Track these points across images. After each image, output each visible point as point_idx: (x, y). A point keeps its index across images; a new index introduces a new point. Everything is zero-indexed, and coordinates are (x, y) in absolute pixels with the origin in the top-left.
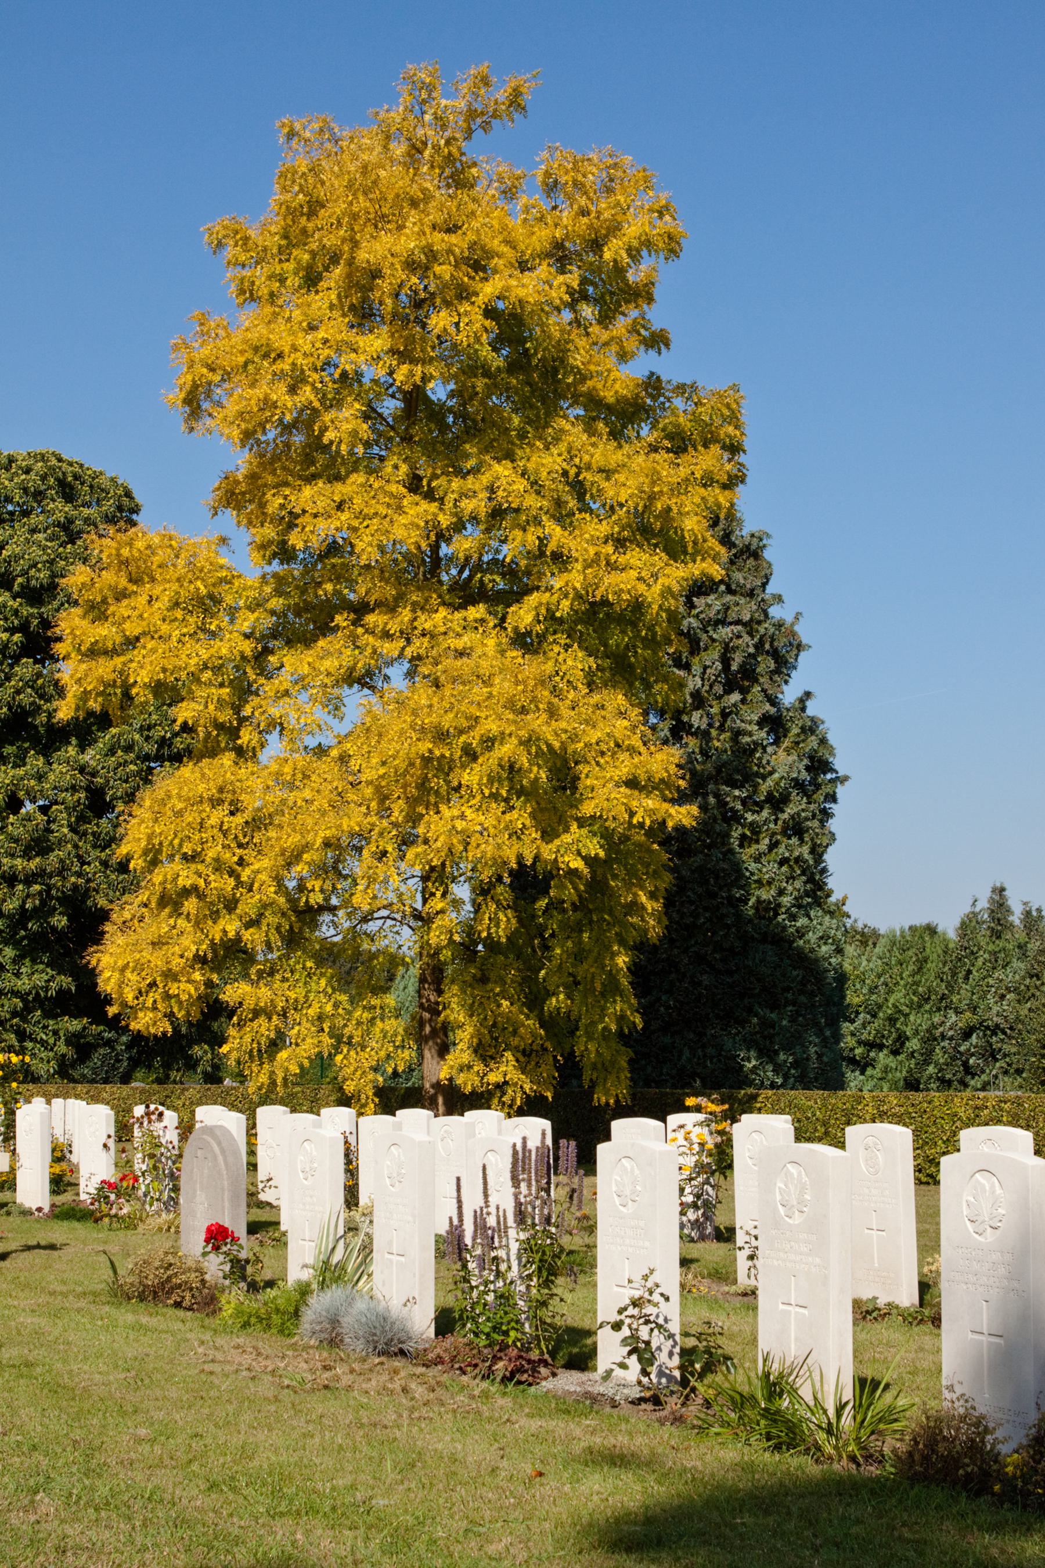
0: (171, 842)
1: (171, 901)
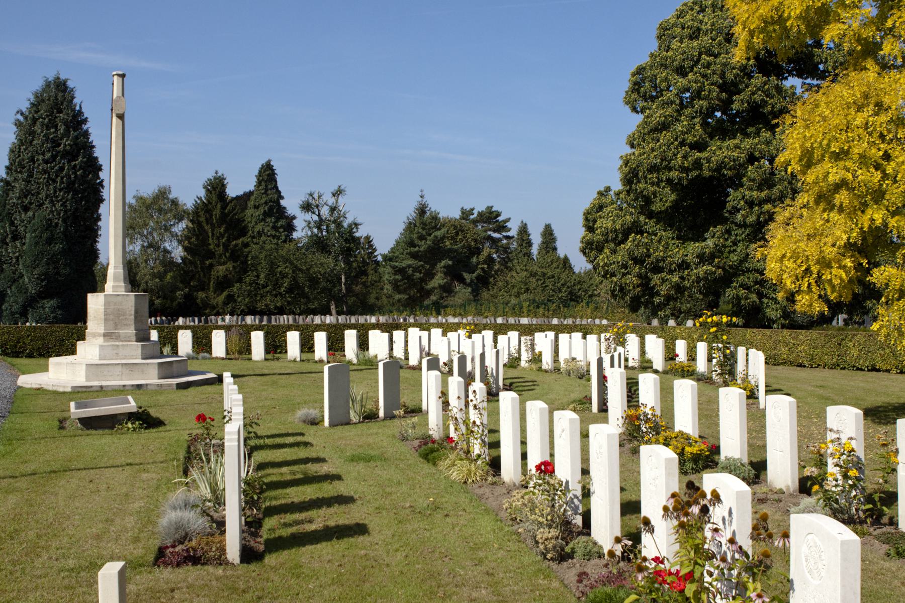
0: (821, 143)
1: (825, 199)
